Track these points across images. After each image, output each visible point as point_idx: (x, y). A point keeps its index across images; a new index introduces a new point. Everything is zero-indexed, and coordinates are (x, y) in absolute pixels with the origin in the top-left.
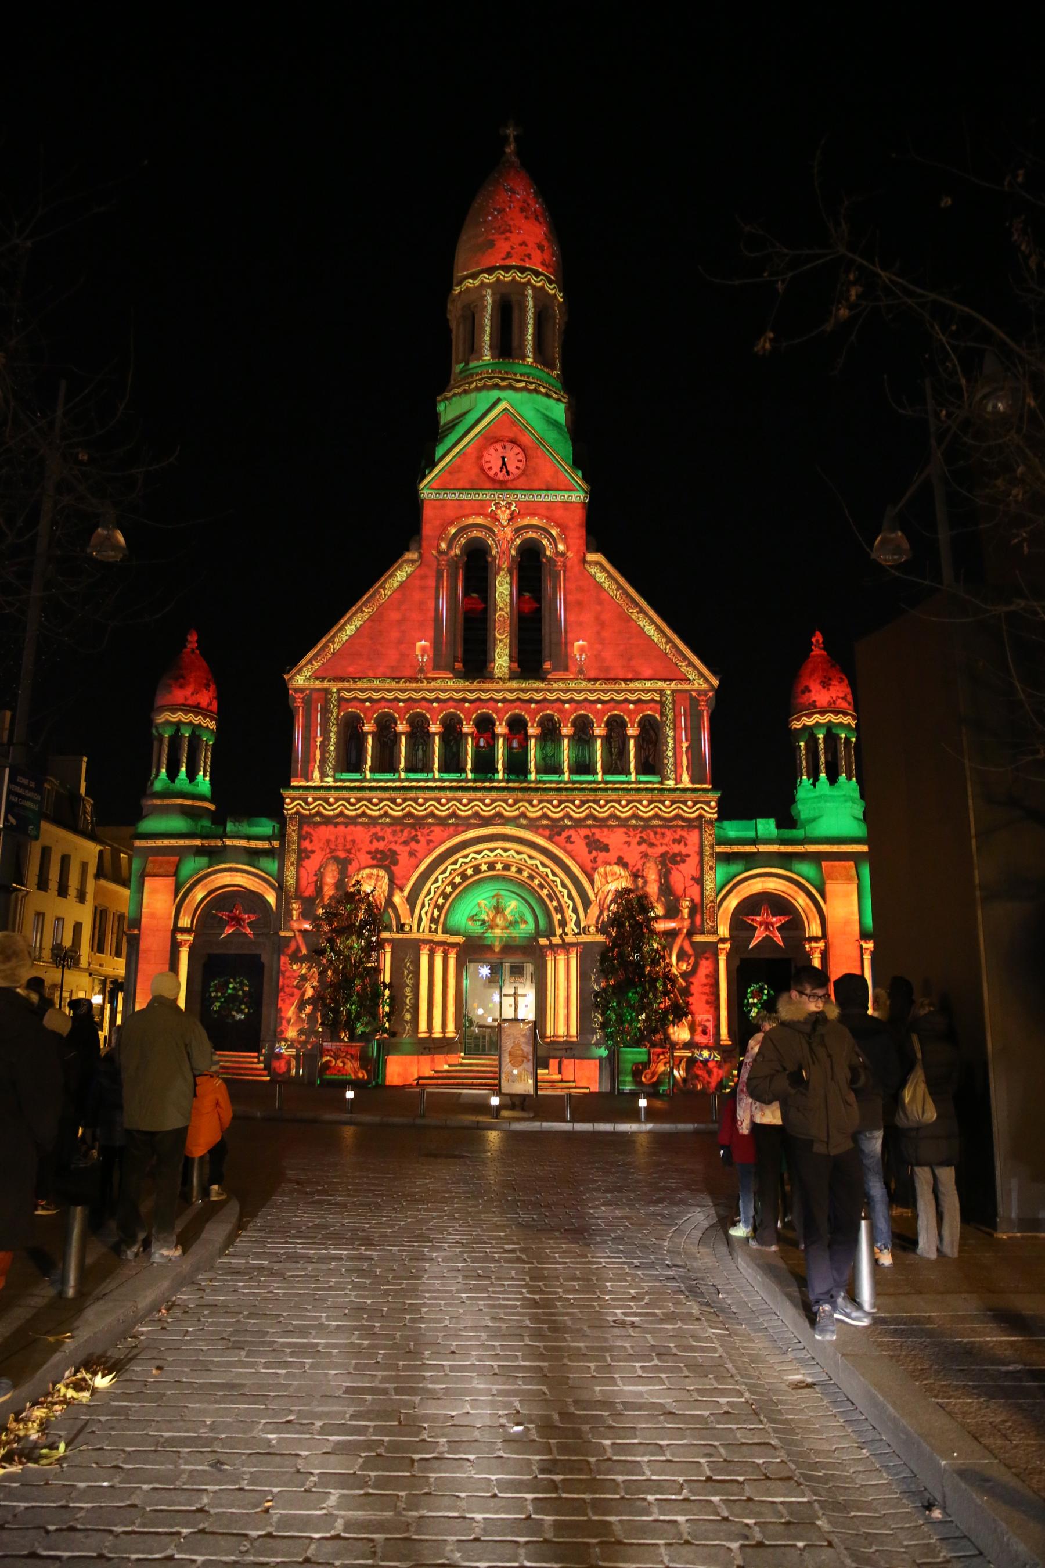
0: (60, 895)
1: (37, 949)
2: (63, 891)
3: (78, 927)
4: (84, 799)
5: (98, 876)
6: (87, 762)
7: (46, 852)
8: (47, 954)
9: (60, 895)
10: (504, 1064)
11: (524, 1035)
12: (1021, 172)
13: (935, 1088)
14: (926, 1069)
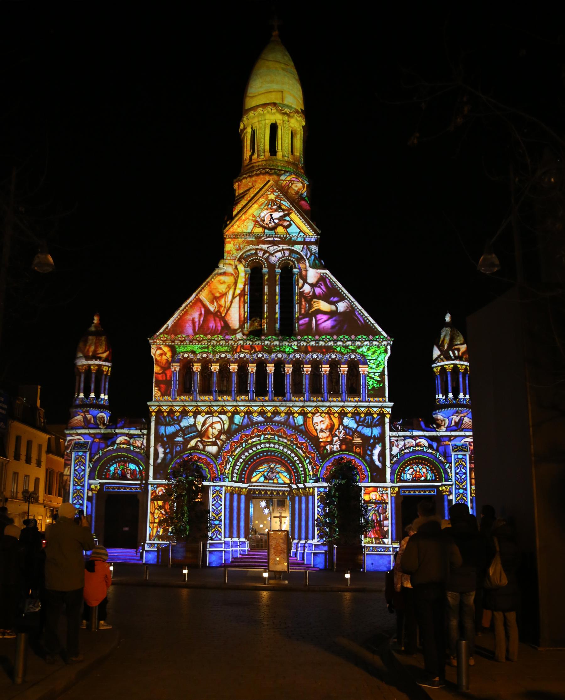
3: (37, 480)
4: (39, 409)
6: (41, 389)
7: (18, 439)
8: (20, 495)
10: (271, 554)
11: (282, 539)
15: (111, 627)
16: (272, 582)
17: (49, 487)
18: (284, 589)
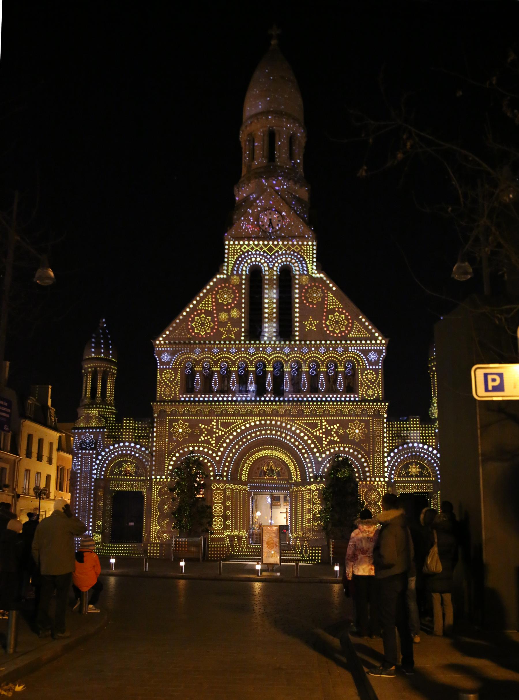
0: (38, 460)
1: (27, 489)
2: (40, 458)
3: (48, 477)
4: (50, 409)
5: (59, 450)
6: (52, 389)
7: (30, 437)
8: (32, 492)
9: (38, 460)
10: (264, 548)
11: (274, 533)
12: (495, 78)
13: (442, 555)
14: (439, 547)
15: (99, 611)
16: (265, 574)
17: (60, 483)
18: (276, 580)
